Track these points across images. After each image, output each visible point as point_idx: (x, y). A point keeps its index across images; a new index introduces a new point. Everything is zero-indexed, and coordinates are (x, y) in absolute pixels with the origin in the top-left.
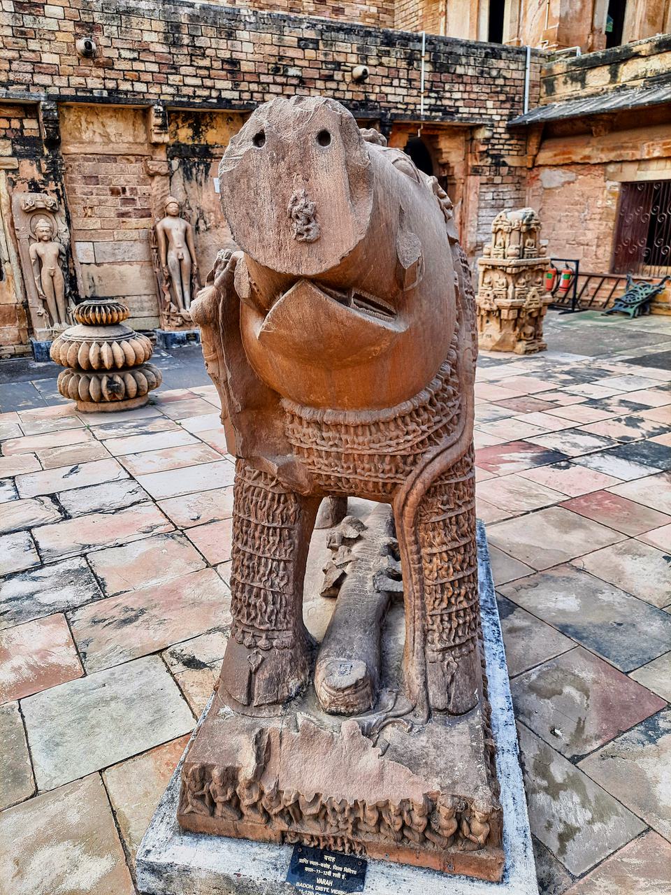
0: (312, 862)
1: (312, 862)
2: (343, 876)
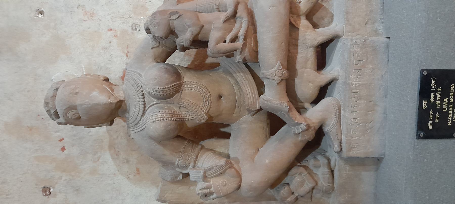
0: (431, 117)
1: (431, 117)
2: (439, 90)
